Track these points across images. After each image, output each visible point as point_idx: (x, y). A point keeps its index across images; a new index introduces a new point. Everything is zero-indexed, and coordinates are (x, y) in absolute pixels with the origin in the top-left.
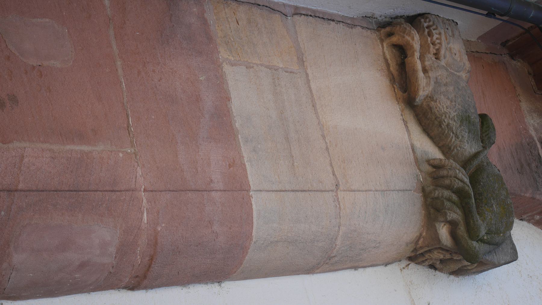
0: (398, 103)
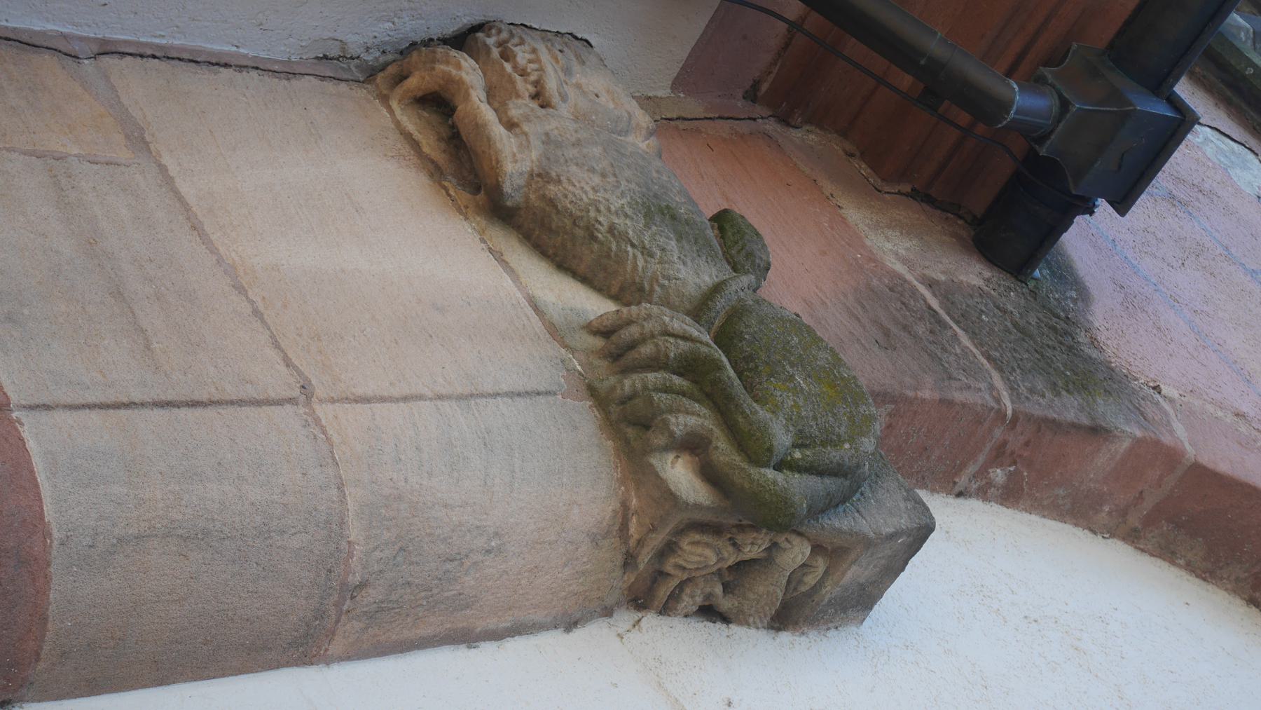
0: (466, 219)
